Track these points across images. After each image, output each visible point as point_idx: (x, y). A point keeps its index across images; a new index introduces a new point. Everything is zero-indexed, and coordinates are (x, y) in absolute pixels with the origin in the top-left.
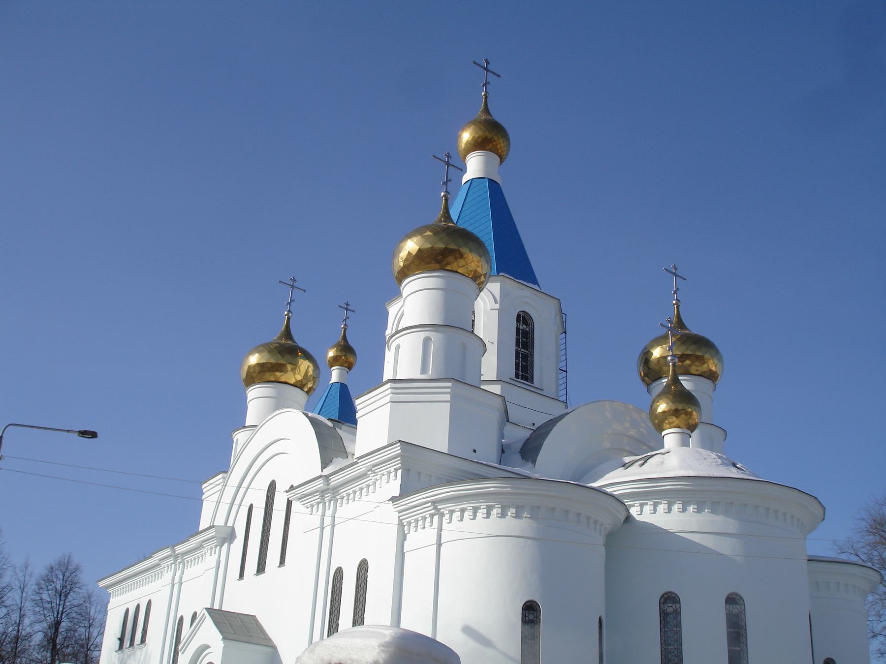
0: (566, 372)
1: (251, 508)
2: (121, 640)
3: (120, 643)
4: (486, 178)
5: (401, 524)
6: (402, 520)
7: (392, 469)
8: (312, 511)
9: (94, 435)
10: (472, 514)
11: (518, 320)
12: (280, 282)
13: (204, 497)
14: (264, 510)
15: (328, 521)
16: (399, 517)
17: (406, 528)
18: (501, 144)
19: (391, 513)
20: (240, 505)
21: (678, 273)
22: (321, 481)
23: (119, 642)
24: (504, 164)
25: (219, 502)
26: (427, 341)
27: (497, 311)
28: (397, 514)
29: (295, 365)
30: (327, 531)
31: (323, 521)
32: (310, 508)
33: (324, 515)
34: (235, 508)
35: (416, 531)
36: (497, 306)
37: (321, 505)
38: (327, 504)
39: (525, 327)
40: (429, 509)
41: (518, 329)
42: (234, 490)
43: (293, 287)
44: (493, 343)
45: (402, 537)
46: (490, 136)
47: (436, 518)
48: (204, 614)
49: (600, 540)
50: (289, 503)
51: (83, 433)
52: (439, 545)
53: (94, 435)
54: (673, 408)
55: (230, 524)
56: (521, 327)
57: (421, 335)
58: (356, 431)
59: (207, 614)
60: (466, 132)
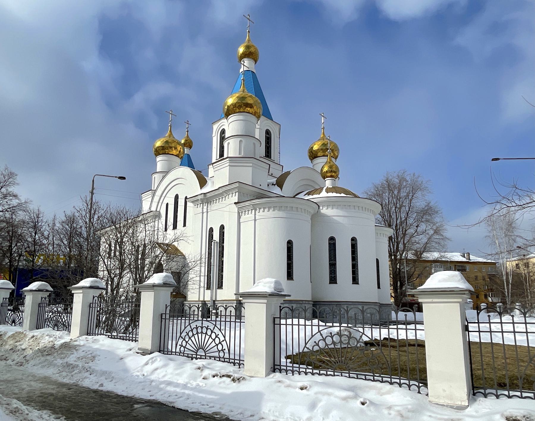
1: (167, 205)
5: (239, 213)
7: (234, 192)
9: (124, 178)
13: (143, 199)
15: (205, 210)
17: (241, 214)
19: (235, 208)
24: (257, 63)
26: (241, 141)
27: (514, 344)
28: (237, 209)
30: (205, 214)
31: (203, 210)
33: (203, 208)
37: (201, 205)
38: (204, 204)
42: (159, 197)
45: (239, 217)
47: (253, 211)
52: (255, 220)
53: (124, 178)
54: (330, 170)
58: (185, 166)
60: (241, 47)
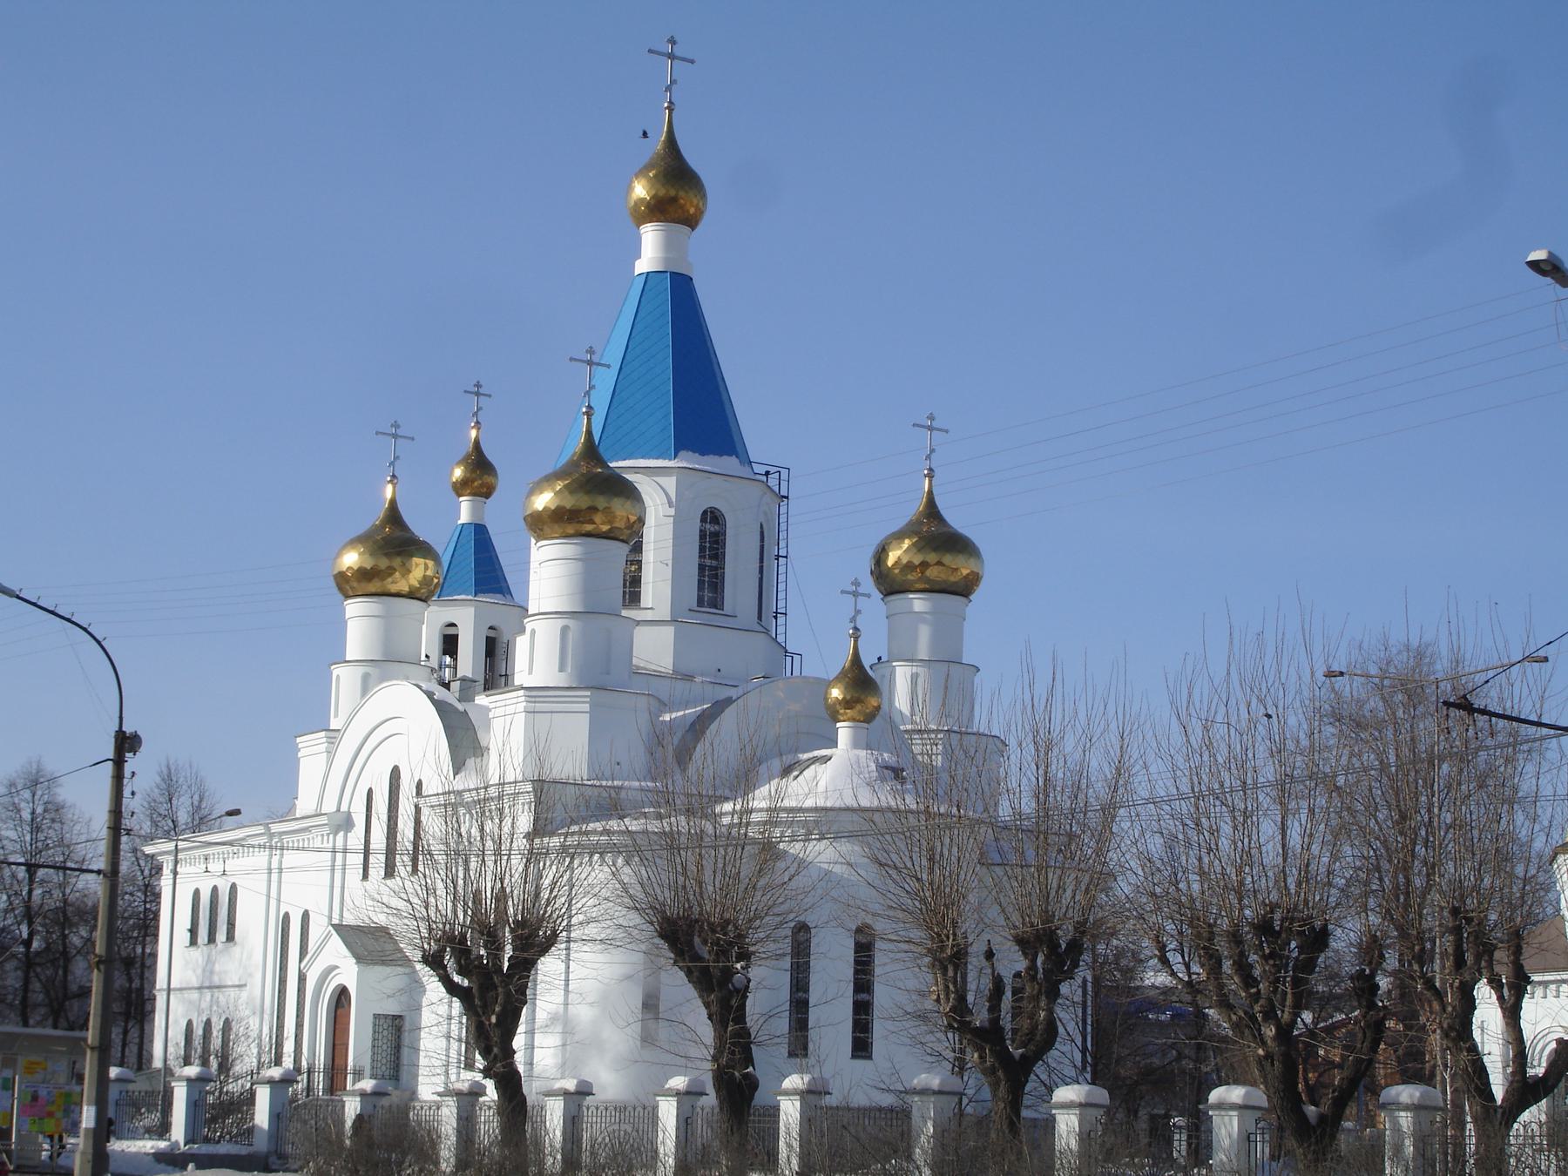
0: (786, 557)
1: (370, 792)
2: (193, 931)
3: (191, 935)
4: (666, 272)
11: (703, 520)
12: (377, 433)
18: (689, 201)
21: (935, 424)
23: (189, 934)
26: (565, 630)
29: (407, 571)
30: (275, 877)
31: (270, 863)
36: (672, 511)
43: (395, 436)
44: (667, 565)
46: (672, 193)
48: (330, 931)
50: (418, 809)
55: (344, 808)
57: (560, 623)
59: (333, 932)
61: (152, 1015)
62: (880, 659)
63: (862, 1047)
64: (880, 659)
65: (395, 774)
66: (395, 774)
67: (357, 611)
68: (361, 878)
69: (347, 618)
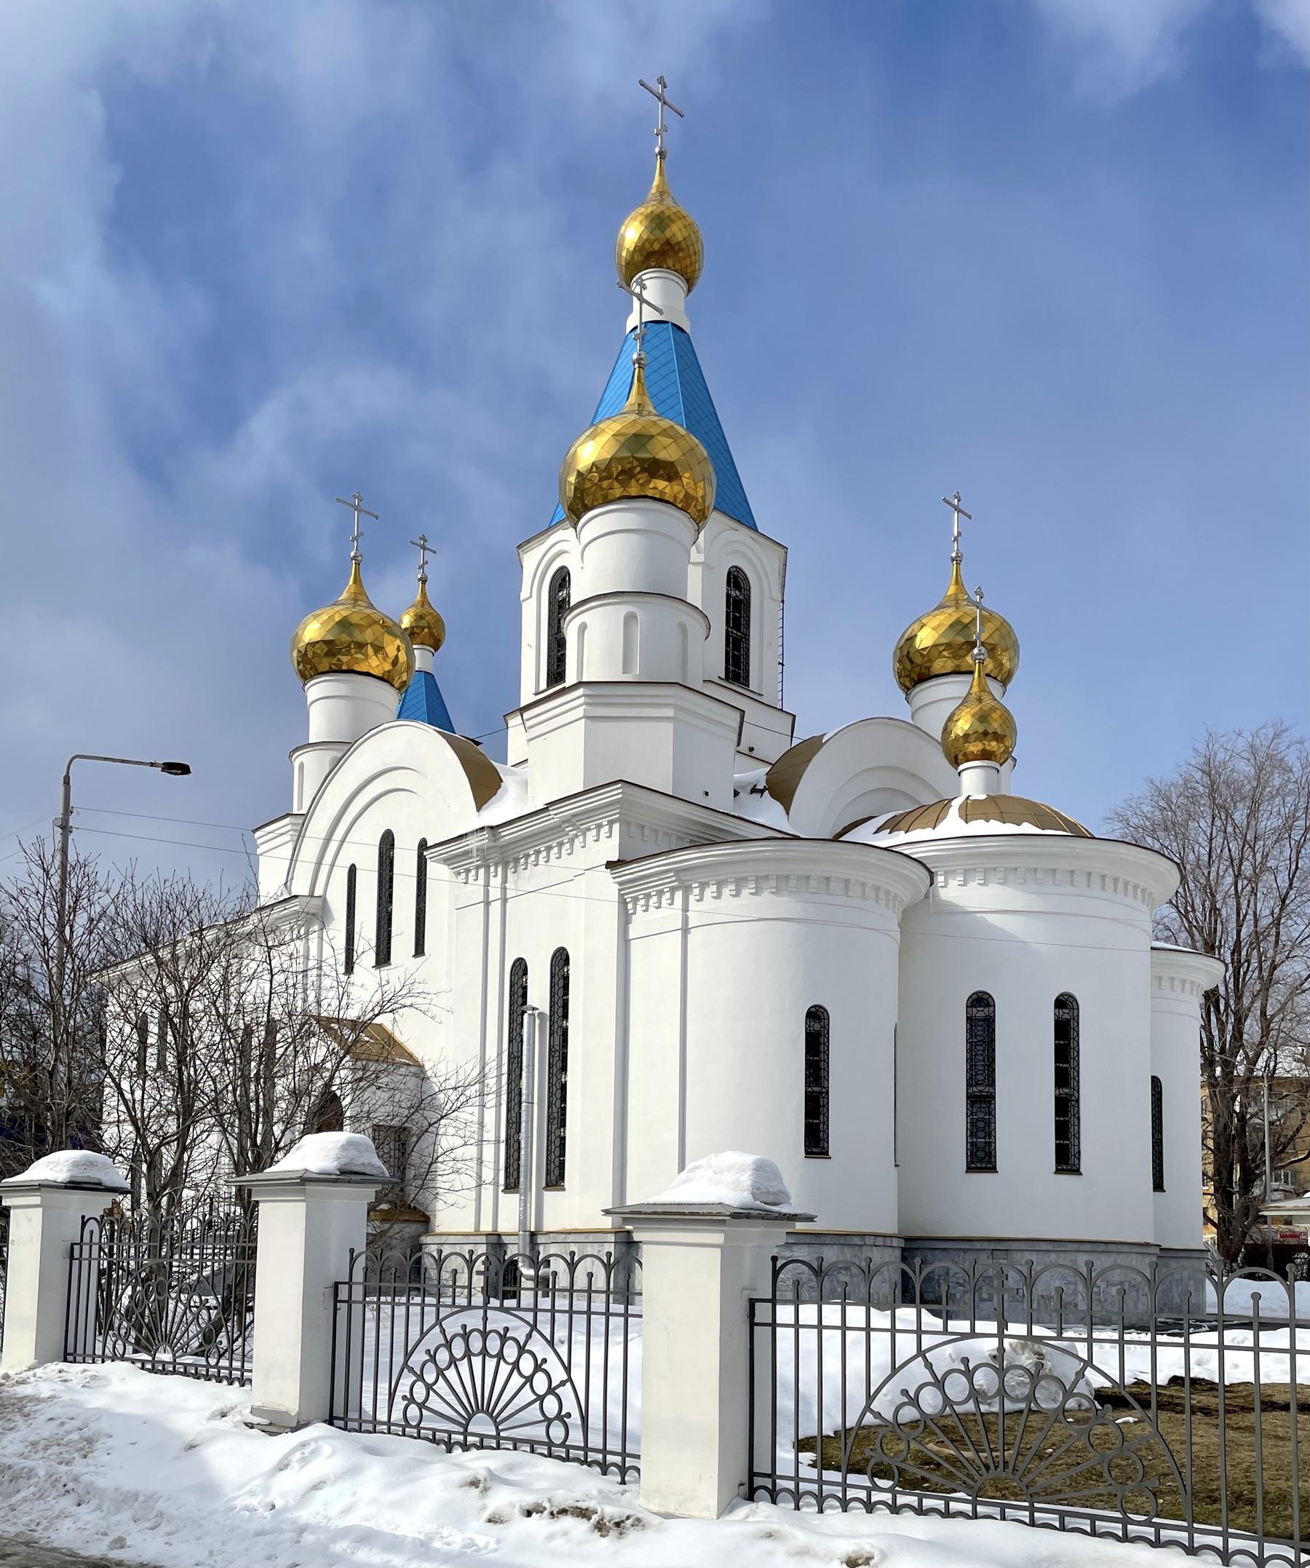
1: (352, 871)
5: (623, 903)
6: (623, 895)
8: (467, 877)
9: (184, 769)
10: (734, 888)
13: (259, 852)
14: (377, 874)
15: (495, 893)
16: (620, 890)
17: (630, 906)
20: (332, 865)
22: (486, 834)
25: (292, 860)
26: (630, 618)
30: (496, 908)
31: (487, 893)
32: (463, 875)
33: (487, 885)
34: (324, 870)
35: (646, 910)
38: (492, 869)
39: (738, 593)
40: (671, 879)
41: (728, 596)
45: (625, 919)
49: (891, 921)
51: (171, 768)
52: (686, 930)
53: (184, 769)
55: (318, 892)
56: (733, 593)
57: (617, 612)
61: (428, 1138)
62: (779, 663)
63: (1067, 1159)
64: (779, 663)
65: (387, 842)
66: (387, 842)
67: (317, 689)
68: (413, 954)
69: (521, 599)
